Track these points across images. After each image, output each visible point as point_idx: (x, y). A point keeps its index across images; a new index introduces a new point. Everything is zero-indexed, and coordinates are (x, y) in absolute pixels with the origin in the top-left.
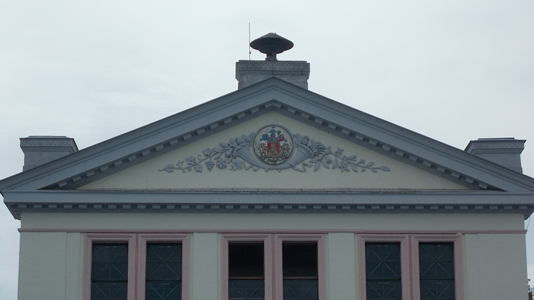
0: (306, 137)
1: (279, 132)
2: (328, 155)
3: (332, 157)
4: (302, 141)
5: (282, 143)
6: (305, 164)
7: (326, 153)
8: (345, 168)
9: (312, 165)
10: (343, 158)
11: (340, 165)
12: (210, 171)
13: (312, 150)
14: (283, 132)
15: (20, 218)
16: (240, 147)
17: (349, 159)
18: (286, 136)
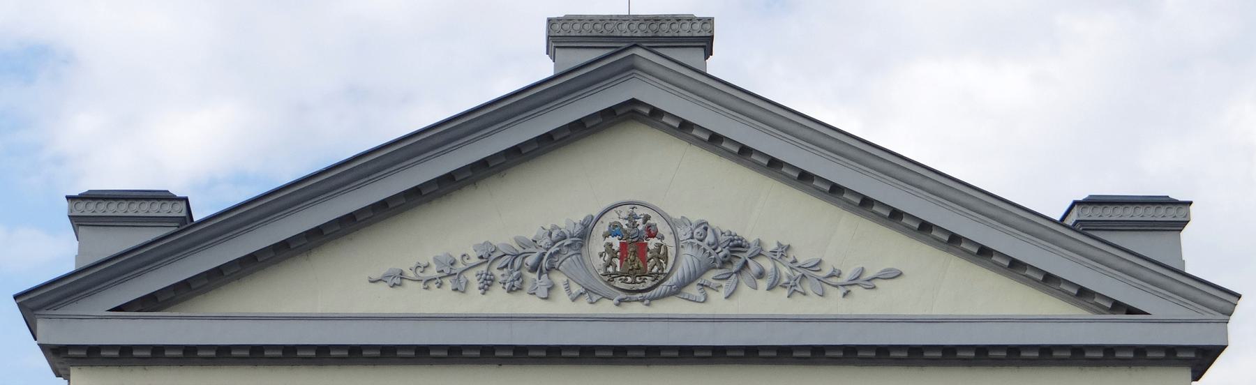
0: (703, 223)
1: (647, 218)
2: (756, 260)
3: (767, 264)
4: (693, 233)
5: (652, 243)
6: (702, 285)
7: (752, 254)
8: (793, 288)
9: (721, 286)
10: (791, 265)
11: (785, 280)
12: (483, 294)
13: (717, 251)
14: (655, 220)
15: (69, 375)
16: (558, 249)
17: (804, 266)
18: (663, 228)
